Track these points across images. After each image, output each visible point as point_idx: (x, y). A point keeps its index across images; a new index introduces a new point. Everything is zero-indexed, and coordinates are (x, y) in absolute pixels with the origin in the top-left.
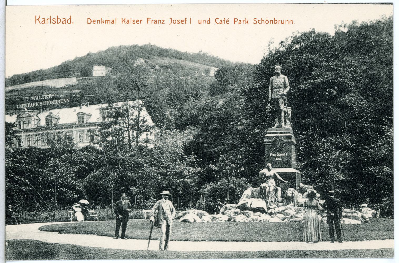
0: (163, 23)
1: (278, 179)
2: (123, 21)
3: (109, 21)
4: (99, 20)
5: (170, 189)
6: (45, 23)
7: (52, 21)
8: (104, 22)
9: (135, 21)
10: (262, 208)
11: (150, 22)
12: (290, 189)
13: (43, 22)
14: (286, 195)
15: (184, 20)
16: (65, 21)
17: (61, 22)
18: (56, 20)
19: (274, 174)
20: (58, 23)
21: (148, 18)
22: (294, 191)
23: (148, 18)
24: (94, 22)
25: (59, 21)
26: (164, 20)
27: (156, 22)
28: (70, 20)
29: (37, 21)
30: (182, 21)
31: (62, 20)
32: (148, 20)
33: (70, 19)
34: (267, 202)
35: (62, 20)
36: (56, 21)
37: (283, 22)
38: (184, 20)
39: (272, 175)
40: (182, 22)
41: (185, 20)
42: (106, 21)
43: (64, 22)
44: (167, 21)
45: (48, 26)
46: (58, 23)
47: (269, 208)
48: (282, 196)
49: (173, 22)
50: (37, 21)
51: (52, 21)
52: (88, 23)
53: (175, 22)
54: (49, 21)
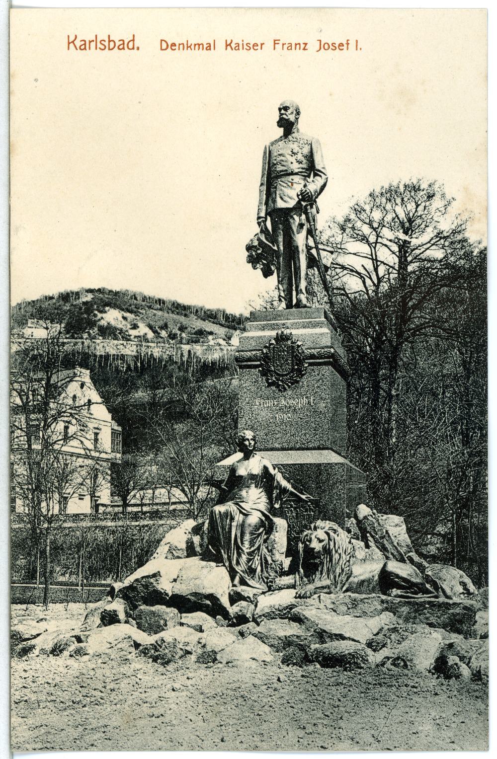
0: (304, 49)
1: (279, 486)
2: (228, 45)
3: (201, 46)
4: (183, 44)
5: (423, 434)
6: (239, 49)
7: (99, 45)
8: (193, 47)
9: (337, 45)
10: (212, 597)
11: (279, 47)
12: (319, 523)
13: (83, 47)
14: (306, 547)
15: (345, 43)
16: (124, 44)
17: (116, 47)
18: (106, 44)
19: (265, 468)
20: (109, 49)
21: (275, 41)
22: (335, 531)
23: (275, 41)
24: (173, 48)
25: (112, 44)
26: (306, 44)
27: (290, 47)
28: (132, 43)
29: (72, 45)
30: (341, 45)
31: (118, 44)
32: (275, 44)
33: (133, 40)
34: (233, 573)
35: (118, 44)
36: (109, 44)
37: (298, 46)
38: (345, 43)
39: (257, 470)
40: (255, 48)
41: (348, 44)
42: (195, 45)
43: (121, 47)
44: (313, 46)
45: (93, 53)
46: (109, 49)
47: (235, 598)
48: (291, 551)
49: (323, 46)
50: (72, 45)
51: (99, 45)
52: (162, 49)
53: (326, 46)
54: (93, 44)
